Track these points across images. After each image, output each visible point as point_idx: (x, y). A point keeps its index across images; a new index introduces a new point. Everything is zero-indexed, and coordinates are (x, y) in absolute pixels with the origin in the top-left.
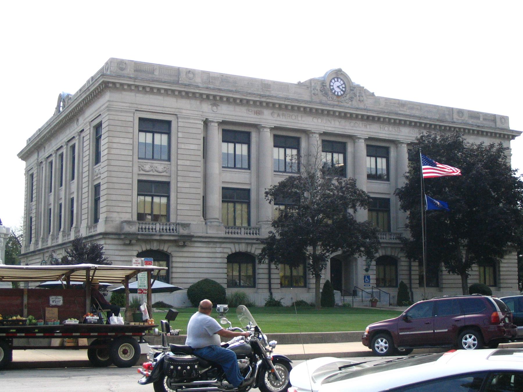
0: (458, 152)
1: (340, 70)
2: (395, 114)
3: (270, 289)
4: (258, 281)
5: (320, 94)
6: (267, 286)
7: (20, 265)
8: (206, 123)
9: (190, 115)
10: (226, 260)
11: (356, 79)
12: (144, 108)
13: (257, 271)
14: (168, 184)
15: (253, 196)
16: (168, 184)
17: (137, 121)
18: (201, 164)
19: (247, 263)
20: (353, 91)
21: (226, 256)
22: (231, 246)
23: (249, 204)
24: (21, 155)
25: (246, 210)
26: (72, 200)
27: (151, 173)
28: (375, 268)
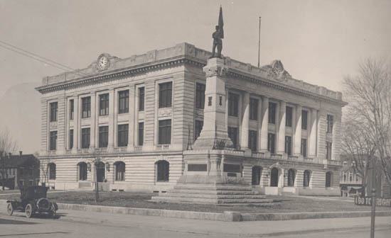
17: (157, 86)
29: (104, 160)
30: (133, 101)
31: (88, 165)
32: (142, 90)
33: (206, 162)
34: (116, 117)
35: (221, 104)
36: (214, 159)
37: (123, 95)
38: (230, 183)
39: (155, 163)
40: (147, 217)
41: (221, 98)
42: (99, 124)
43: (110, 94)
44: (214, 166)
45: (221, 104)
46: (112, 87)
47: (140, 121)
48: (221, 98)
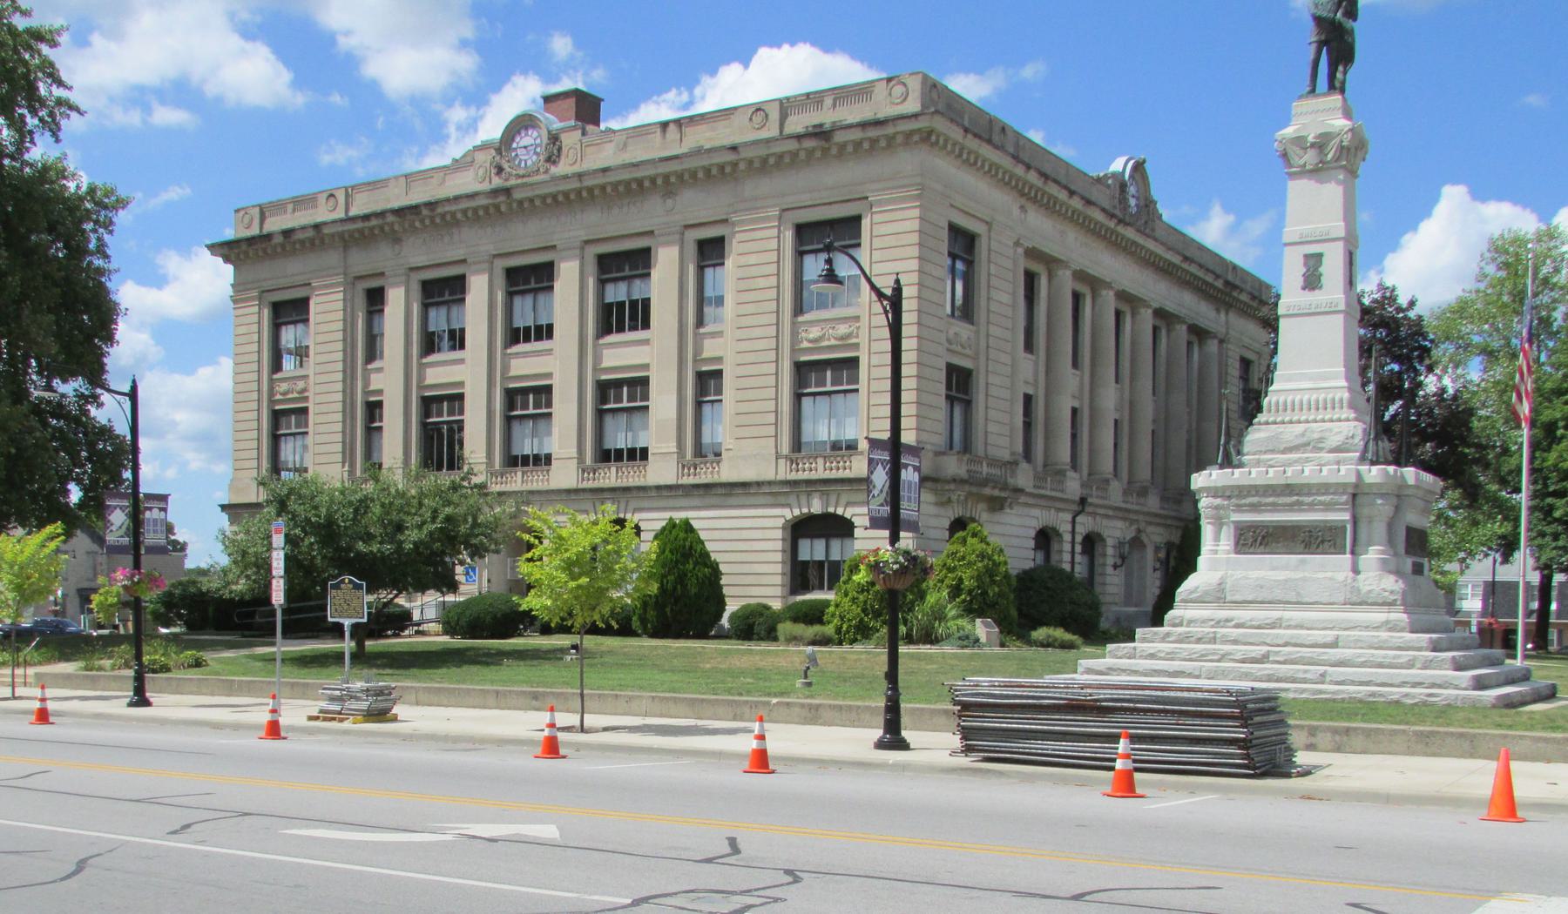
9: (1011, 227)
10: (1032, 544)
26: (374, 409)
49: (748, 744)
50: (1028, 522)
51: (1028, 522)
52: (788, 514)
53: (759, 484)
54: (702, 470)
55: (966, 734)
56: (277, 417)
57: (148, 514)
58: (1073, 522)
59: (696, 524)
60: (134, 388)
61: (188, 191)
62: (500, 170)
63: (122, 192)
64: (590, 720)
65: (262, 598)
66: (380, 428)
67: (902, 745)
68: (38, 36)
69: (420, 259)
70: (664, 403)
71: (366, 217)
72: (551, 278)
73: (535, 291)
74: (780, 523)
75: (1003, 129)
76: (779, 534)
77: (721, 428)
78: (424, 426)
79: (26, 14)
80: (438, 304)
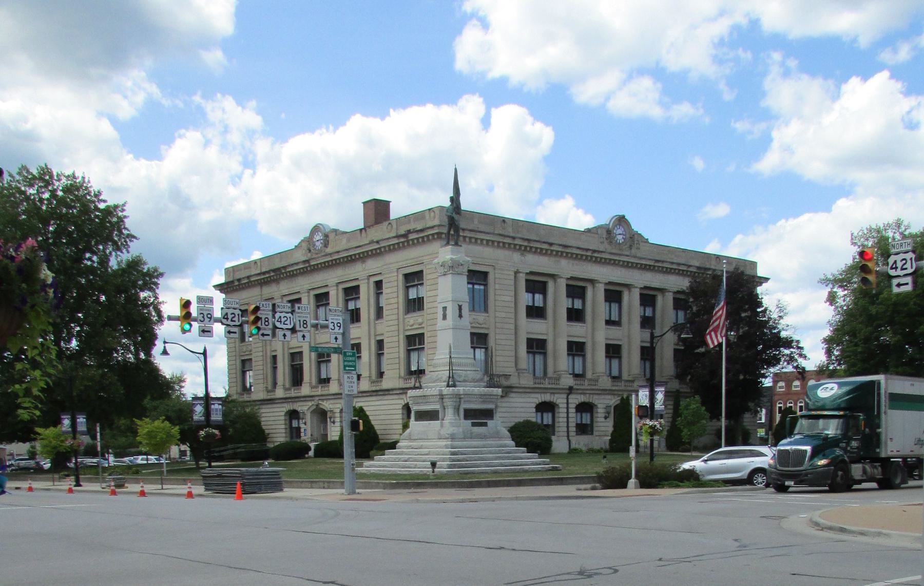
0: (126, 336)
1: (623, 217)
2: (665, 261)
3: (568, 436)
4: (557, 429)
5: (606, 242)
6: (566, 434)
7: (727, 418)
8: (516, 273)
9: (507, 267)
10: (534, 410)
11: (637, 226)
12: (404, 264)
13: (557, 420)
14: (486, 335)
15: (550, 346)
16: (486, 335)
17: (401, 277)
18: (513, 316)
19: (547, 411)
20: (634, 239)
21: (534, 405)
22: (538, 396)
23: (545, 354)
24: (645, 292)
25: (542, 362)
26: (274, 358)
27: (415, 327)
28: (574, 415)
29: (326, 405)
30: (365, 302)
31: (329, 415)
32: (379, 284)
33: (436, 407)
34: (372, 324)
35: (460, 316)
36: (448, 402)
37: (352, 292)
38: (472, 437)
39: (287, 413)
40: (113, 497)
41: (460, 307)
42: (376, 335)
43: (331, 293)
44: (450, 413)
45: (460, 316)
46: (332, 280)
47: (379, 338)
48: (460, 307)
49: (28, 486)
50: (531, 400)
51: (531, 400)
52: (285, 410)
53: (392, 390)
54: (245, 396)
55: (205, 485)
56: (244, 362)
57: (213, 406)
58: (567, 399)
59: (365, 409)
60: (205, 351)
61: (707, 120)
62: (310, 251)
63: (161, 270)
64: (165, 487)
65: (95, 447)
66: (766, 310)
67: (80, 486)
68: (116, 207)
69: (286, 292)
70: (367, 355)
71: (268, 272)
72: (328, 299)
73: (417, 285)
74: (283, 414)
75: (504, 221)
76: (400, 412)
77: (250, 378)
78: (292, 366)
79: (105, 201)
80: (322, 305)
